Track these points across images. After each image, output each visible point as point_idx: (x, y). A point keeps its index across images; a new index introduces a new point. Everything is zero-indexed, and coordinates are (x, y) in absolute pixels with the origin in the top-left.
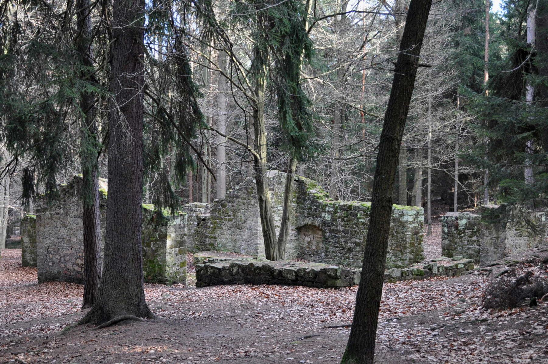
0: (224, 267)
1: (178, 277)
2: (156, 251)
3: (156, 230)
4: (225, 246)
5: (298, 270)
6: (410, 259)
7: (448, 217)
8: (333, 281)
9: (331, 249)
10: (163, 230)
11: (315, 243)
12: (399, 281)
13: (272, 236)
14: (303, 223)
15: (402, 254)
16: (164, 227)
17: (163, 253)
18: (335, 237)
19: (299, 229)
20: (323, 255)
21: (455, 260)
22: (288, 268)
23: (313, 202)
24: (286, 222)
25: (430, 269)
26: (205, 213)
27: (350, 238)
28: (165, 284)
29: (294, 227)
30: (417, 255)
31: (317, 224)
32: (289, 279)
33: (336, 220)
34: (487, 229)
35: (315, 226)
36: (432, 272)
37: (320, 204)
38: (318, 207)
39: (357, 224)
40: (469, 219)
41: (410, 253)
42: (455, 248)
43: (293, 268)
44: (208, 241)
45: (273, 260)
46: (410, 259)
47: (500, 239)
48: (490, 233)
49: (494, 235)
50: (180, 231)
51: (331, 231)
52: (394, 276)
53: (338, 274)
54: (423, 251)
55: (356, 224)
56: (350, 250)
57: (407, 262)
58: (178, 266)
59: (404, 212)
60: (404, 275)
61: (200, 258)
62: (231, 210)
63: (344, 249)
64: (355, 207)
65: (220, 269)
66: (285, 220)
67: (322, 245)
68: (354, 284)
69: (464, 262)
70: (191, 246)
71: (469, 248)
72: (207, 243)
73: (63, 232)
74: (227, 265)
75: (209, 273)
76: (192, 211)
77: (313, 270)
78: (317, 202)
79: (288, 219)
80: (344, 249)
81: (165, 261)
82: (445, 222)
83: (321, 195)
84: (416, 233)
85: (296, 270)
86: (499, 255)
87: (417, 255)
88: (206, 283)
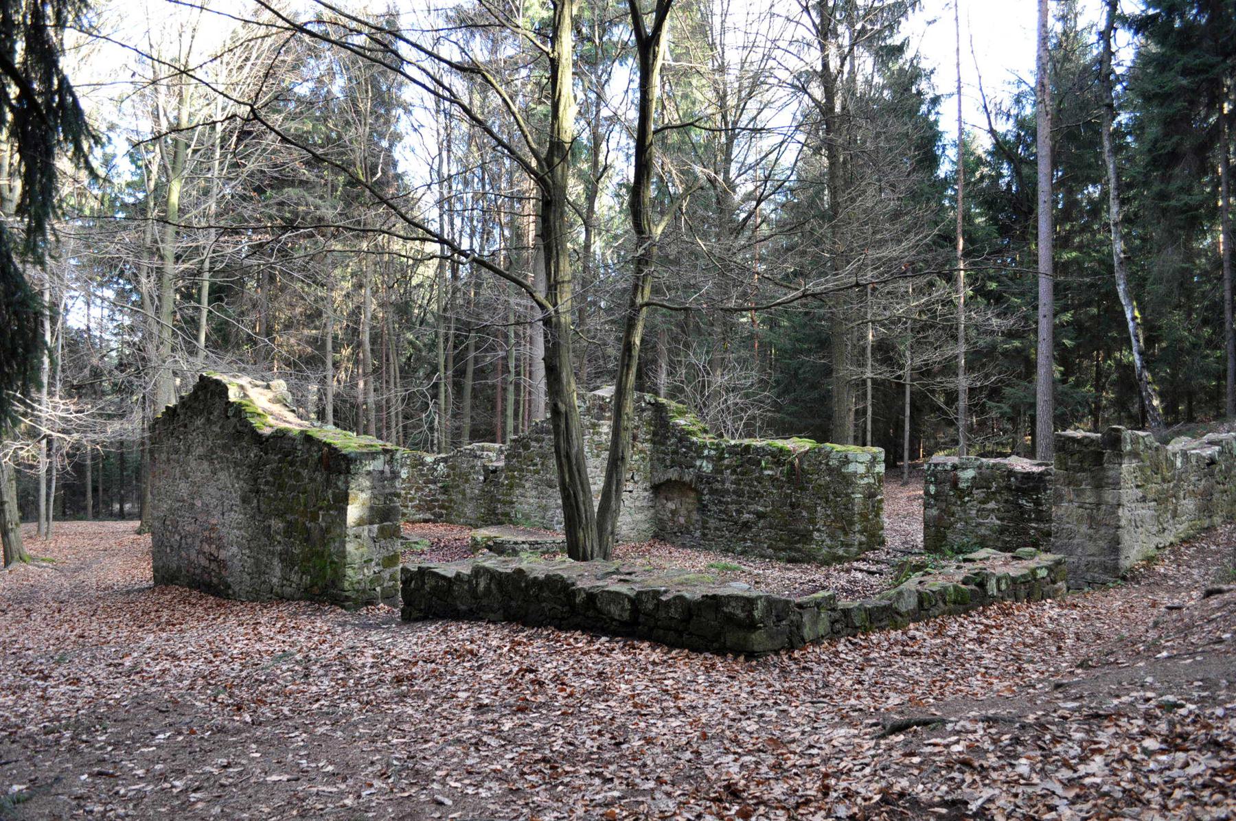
0: (458, 574)
1: (378, 589)
2: (327, 530)
3: (328, 483)
4: (527, 517)
5: (639, 593)
6: (861, 543)
7: (936, 465)
8: (741, 634)
9: (712, 523)
10: (340, 484)
11: (683, 512)
12: (914, 621)
13: (581, 498)
14: (664, 478)
15: (846, 534)
16: (342, 477)
17: (340, 536)
18: (720, 502)
19: (658, 489)
20: (698, 534)
21: (1020, 558)
22: (612, 588)
23: (680, 440)
24: (617, 467)
25: (982, 585)
26: (498, 460)
27: (747, 504)
28: (343, 607)
29: (648, 485)
30: (873, 536)
31: (687, 478)
32: (613, 619)
33: (721, 472)
34: (1069, 484)
35: (684, 484)
36: (985, 591)
37: (693, 443)
38: (689, 448)
39: (760, 480)
40: (980, 467)
41: (861, 533)
42: (952, 524)
43: (623, 589)
44: (500, 508)
45: (585, 559)
46: (861, 543)
47: (1104, 507)
48: (1079, 493)
49: (1089, 498)
50: (384, 487)
51: (713, 492)
52: (903, 610)
53: (757, 614)
54: (882, 529)
55: (757, 479)
56: (746, 526)
57: (854, 550)
58: (378, 564)
59: (850, 457)
60: (926, 605)
61: (479, 539)
62: (537, 455)
63: (736, 523)
64: (757, 449)
65: (450, 579)
66: (615, 463)
67: (695, 516)
68: (803, 640)
69: (1045, 564)
70: (473, 516)
71: (980, 524)
72: (499, 511)
73: (183, 488)
74: (466, 570)
75: (427, 587)
76: (475, 457)
77: (681, 598)
78: (688, 440)
79: (623, 458)
80: (736, 523)
81: (343, 554)
82: (931, 475)
83: (695, 429)
84: (872, 496)
85: (632, 594)
86: (1101, 543)
87: (873, 536)
88: (421, 610)
